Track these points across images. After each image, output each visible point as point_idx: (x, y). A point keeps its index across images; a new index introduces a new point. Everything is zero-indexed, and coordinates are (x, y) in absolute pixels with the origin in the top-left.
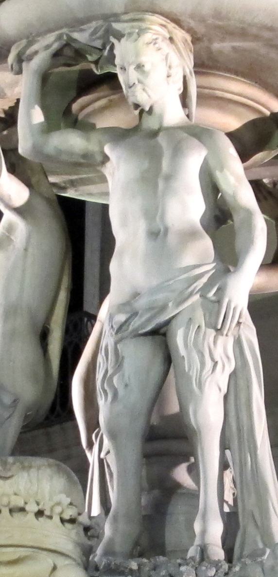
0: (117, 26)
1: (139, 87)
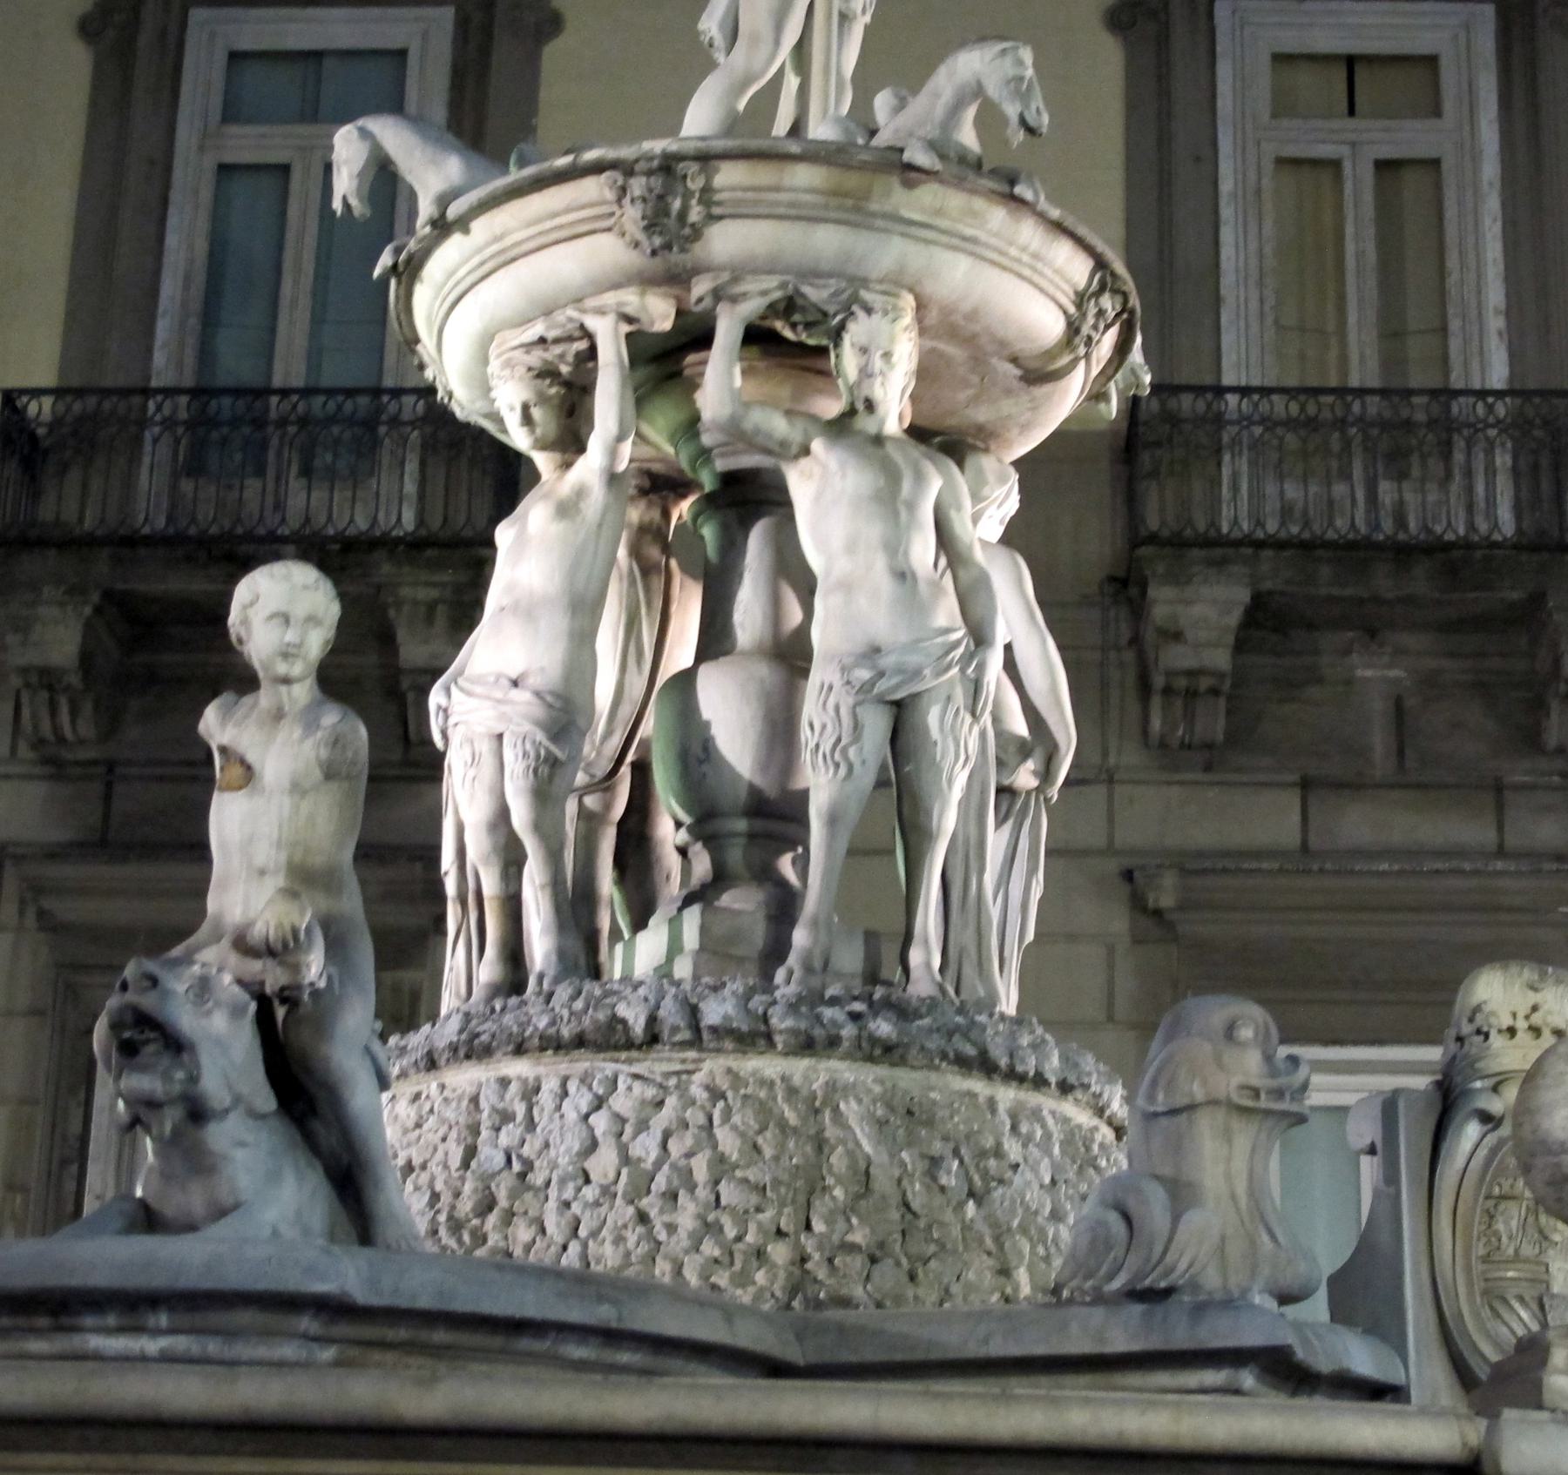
0: (865, 295)
1: (879, 380)
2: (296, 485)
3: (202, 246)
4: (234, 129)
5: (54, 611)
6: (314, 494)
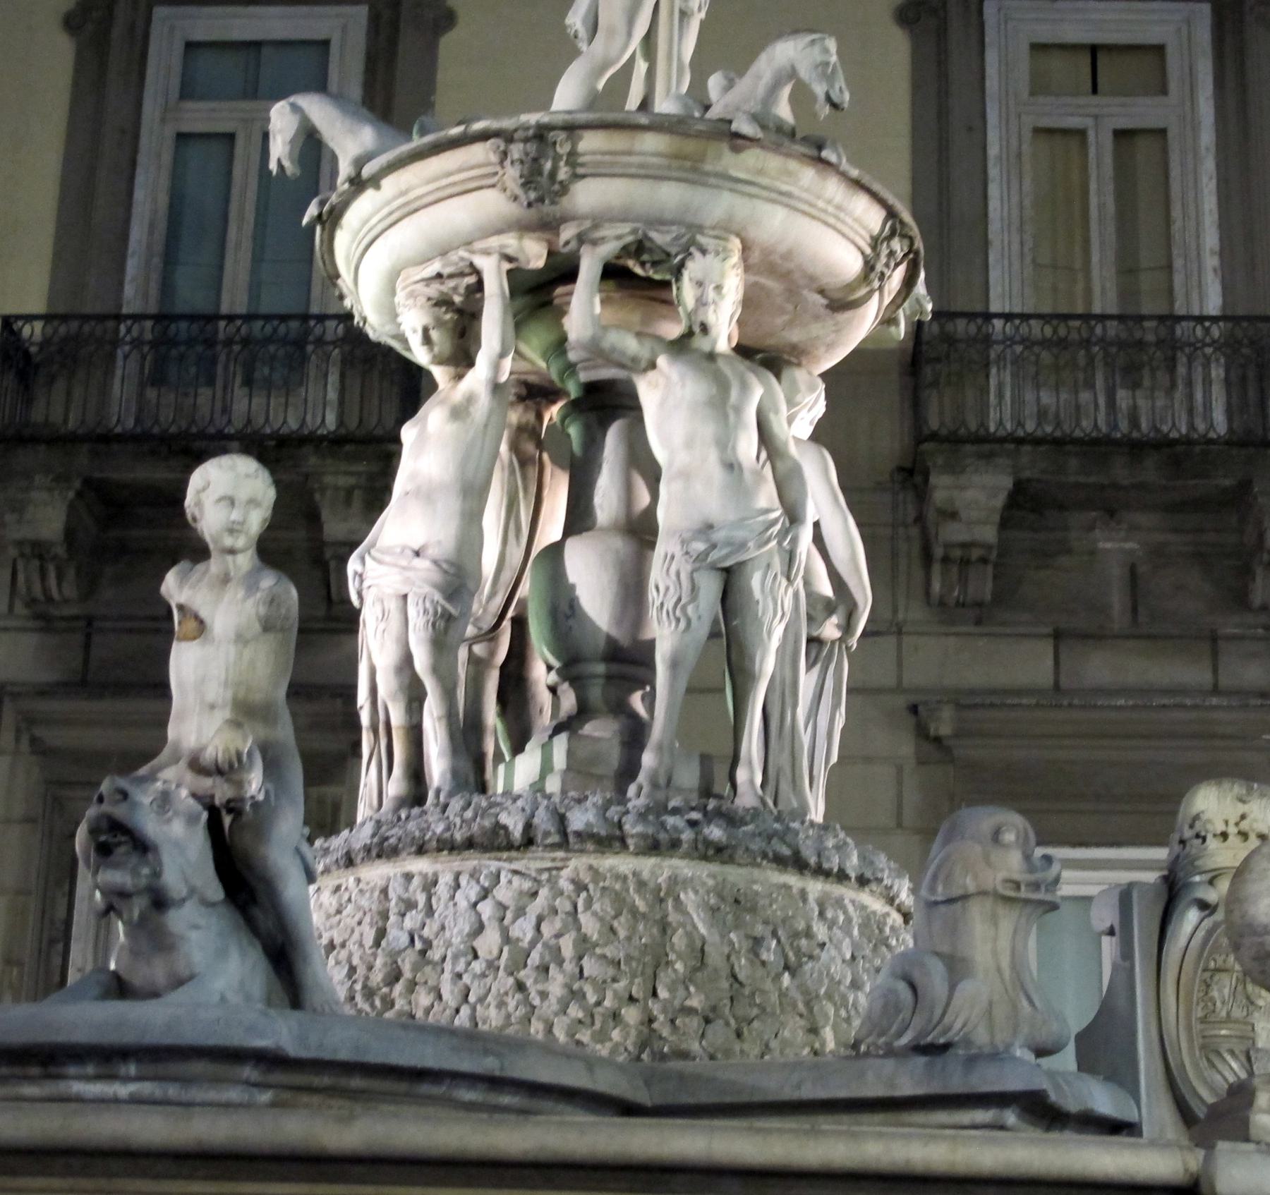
0: (701, 239)
1: (712, 308)
2: (239, 393)
3: (163, 200)
4: (189, 105)
5: (44, 495)
6: (255, 401)
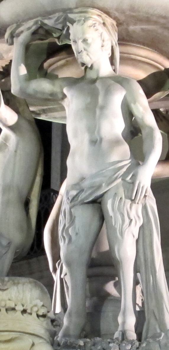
0: (71, 16)
1: (84, 53)
